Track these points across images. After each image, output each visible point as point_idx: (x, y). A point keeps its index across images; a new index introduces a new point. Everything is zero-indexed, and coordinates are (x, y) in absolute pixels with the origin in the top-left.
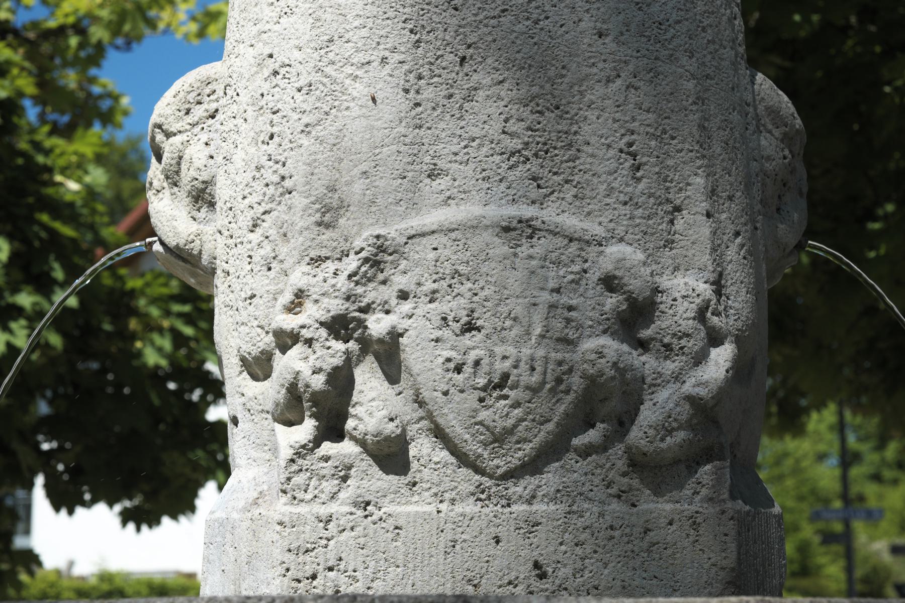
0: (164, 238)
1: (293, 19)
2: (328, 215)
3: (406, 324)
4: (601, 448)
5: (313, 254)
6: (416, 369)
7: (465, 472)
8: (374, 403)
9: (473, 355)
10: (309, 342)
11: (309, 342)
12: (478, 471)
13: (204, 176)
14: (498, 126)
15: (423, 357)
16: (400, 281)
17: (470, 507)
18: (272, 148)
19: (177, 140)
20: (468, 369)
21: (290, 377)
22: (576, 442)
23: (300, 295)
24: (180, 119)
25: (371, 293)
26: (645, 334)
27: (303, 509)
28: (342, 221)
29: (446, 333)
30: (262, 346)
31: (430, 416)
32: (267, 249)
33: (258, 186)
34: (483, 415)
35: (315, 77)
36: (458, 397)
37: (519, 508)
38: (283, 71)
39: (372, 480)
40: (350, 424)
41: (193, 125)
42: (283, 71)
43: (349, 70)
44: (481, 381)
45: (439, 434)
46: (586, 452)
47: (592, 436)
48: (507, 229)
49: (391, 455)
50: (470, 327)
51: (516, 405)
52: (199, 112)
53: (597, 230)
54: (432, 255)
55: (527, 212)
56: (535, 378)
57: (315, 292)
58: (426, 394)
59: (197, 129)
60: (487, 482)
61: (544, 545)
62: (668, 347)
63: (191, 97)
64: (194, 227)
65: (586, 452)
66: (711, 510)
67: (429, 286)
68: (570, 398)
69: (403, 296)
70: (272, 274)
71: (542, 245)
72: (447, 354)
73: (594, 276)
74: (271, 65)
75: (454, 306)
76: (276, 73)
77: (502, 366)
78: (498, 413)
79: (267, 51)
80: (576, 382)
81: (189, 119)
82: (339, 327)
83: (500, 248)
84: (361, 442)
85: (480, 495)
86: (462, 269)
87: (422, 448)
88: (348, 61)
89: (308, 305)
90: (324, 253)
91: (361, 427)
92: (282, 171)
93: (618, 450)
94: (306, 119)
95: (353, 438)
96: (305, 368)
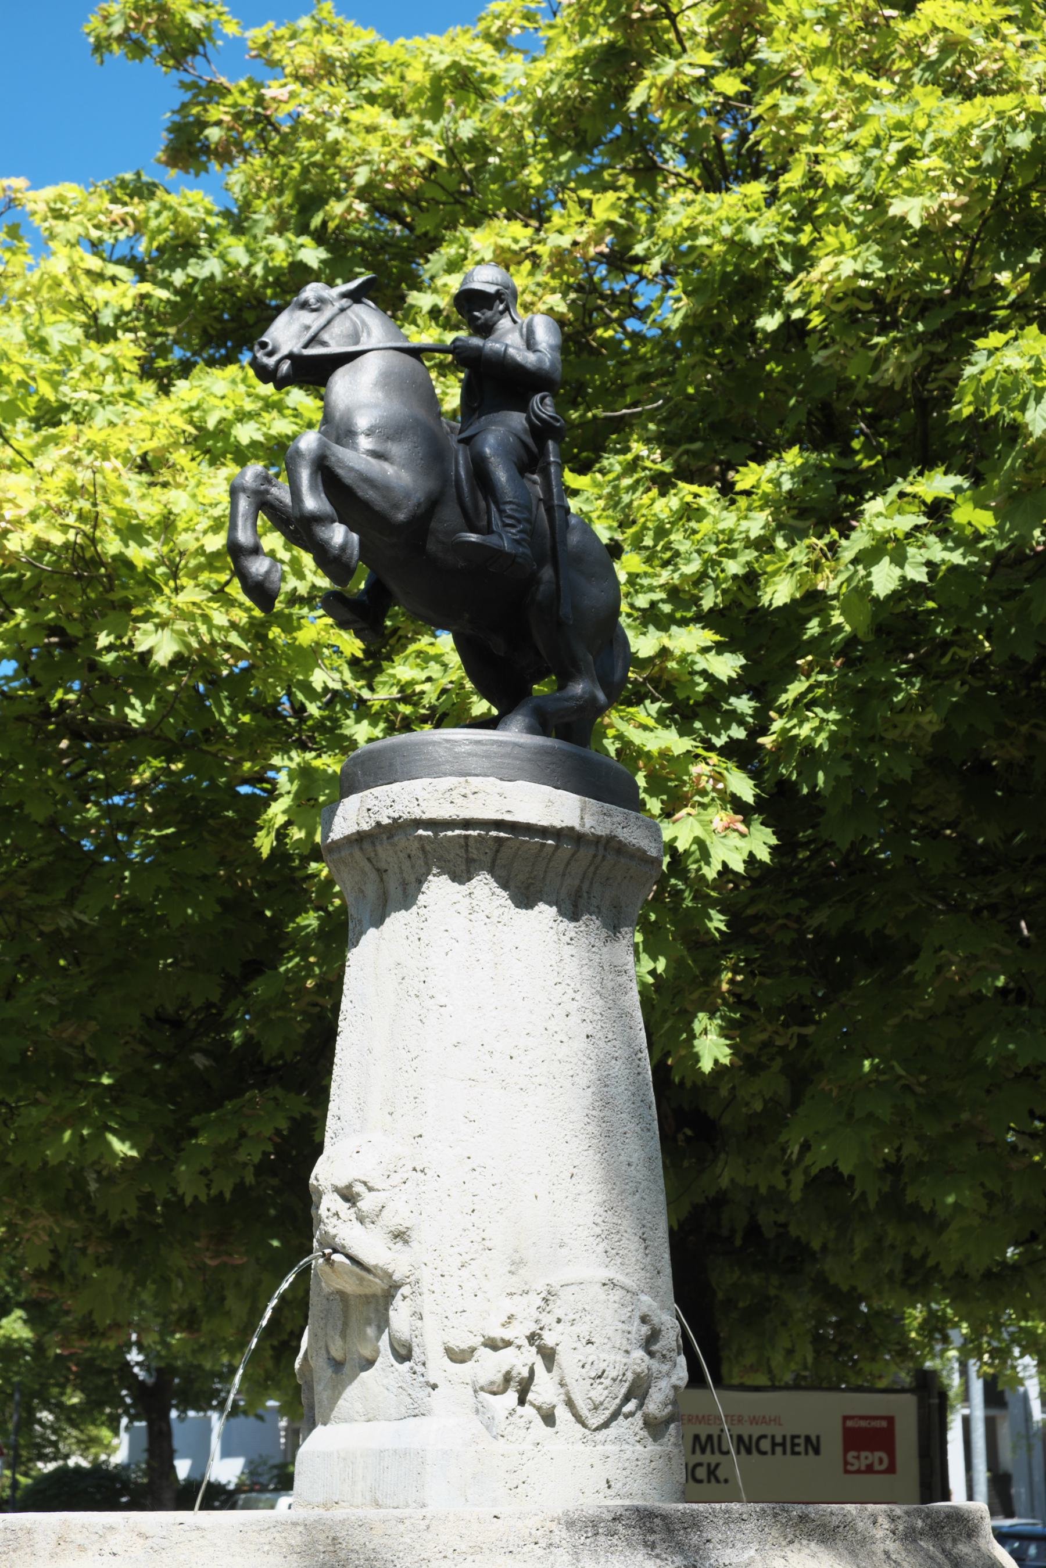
0: (354, 1251)
2: (516, 1265)
3: (561, 1338)
4: (631, 1414)
6: (564, 1365)
8: (544, 1390)
10: (519, 1347)
11: (519, 1347)
12: (584, 1425)
16: (559, 1313)
22: (626, 1409)
25: (547, 1319)
26: (654, 1348)
29: (578, 1345)
31: (567, 1394)
34: (593, 1394)
37: (600, 1447)
40: (530, 1396)
45: (570, 1403)
46: (631, 1414)
47: (631, 1406)
49: (549, 1419)
50: (589, 1342)
52: (396, 1179)
56: (614, 1374)
57: (520, 1316)
58: (568, 1380)
61: (611, 1470)
63: (391, 1167)
65: (627, 1416)
67: (571, 1317)
68: (627, 1385)
69: (559, 1321)
75: (583, 1329)
77: (603, 1366)
78: (599, 1393)
80: (630, 1376)
81: (390, 1181)
82: (532, 1338)
83: (601, 1293)
84: (539, 1409)
85: (584, 1441)
87: (562, 1413)
89: (515, 1322)
93: (639, 1414)
95: (532, 1404)
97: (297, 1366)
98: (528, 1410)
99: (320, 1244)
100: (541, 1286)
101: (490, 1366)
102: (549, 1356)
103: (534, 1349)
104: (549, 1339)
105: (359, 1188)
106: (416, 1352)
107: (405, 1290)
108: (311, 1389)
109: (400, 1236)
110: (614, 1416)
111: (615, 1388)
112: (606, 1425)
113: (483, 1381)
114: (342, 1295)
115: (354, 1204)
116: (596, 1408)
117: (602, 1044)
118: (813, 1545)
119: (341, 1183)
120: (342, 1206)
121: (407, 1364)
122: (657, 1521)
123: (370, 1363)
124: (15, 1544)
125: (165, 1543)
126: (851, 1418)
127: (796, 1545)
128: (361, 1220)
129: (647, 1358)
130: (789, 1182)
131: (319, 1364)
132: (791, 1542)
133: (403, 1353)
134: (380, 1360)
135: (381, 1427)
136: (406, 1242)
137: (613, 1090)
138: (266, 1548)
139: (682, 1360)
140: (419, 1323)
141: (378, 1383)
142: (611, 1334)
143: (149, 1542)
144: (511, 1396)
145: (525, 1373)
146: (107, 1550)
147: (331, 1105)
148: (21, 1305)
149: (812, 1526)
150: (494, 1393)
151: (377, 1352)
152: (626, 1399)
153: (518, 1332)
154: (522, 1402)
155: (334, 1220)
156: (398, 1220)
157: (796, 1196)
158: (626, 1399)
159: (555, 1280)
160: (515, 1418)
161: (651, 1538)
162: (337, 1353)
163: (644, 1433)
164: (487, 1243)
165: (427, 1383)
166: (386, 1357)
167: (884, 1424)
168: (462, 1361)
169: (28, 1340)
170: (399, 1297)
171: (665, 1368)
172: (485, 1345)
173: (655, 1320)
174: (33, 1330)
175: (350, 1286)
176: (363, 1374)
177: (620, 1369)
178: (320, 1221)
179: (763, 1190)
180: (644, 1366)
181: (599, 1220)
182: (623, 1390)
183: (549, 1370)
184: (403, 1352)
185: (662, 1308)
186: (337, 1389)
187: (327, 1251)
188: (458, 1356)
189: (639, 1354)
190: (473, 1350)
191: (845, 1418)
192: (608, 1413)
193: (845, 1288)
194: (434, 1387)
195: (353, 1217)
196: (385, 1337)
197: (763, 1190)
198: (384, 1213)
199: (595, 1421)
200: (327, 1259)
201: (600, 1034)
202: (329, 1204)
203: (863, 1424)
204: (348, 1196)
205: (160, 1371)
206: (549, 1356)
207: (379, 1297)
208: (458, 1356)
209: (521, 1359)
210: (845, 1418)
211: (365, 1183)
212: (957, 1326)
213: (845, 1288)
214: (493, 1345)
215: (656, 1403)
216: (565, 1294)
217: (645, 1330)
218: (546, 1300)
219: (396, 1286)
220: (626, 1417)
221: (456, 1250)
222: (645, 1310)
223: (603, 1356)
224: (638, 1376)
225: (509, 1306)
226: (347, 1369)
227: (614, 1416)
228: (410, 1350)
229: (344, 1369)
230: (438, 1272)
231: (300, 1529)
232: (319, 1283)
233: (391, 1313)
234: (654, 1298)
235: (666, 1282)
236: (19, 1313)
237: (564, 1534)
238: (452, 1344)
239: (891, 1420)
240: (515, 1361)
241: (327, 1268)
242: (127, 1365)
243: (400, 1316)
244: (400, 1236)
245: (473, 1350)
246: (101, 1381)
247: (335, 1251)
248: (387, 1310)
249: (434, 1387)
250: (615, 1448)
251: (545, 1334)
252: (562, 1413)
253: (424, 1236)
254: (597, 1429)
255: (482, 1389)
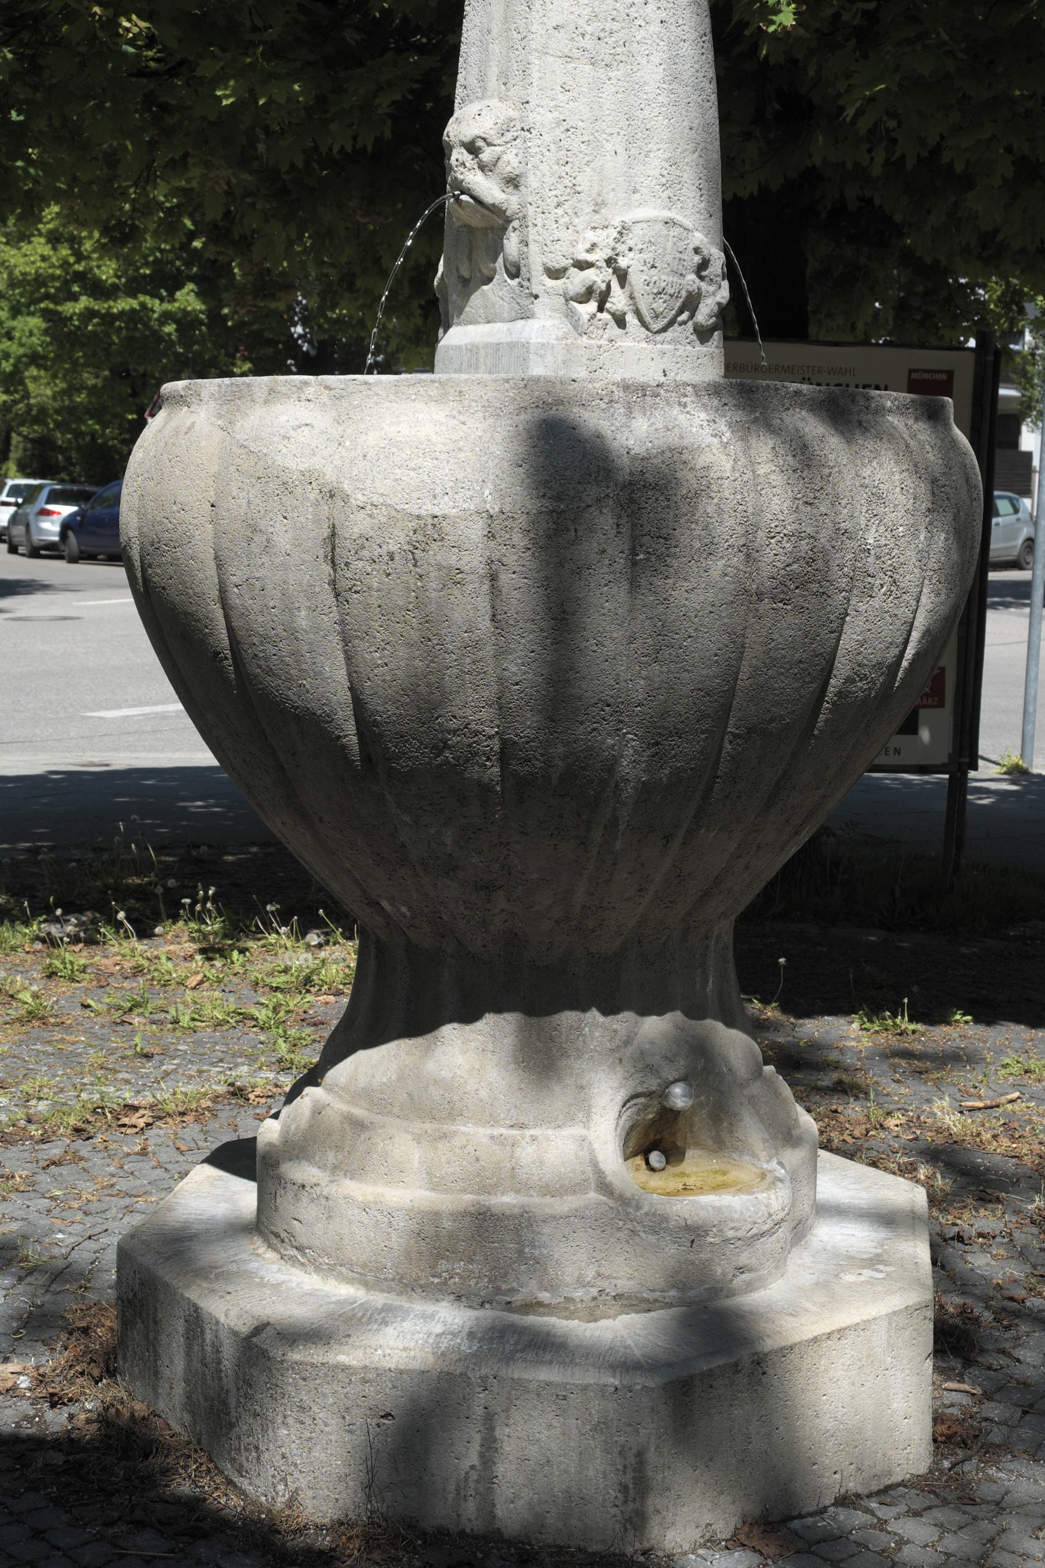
1: (577, 104)
3: (631, 262)
4: (685, 323)
5: (593, 225)
6: (634, 283)
7: (643, 329)
8: (618, 300)
9: (654, 279)
12: (648, 329)
13: (517, 172)
14: (659, 171)
15: (636, 279)
16: (630, 243)
17: (644, 345)
18: (567, 168)
19: (498, 149)
20: (651, 285)
21: (590, 283)
22: (680, 319)
23: (594, 246)
24: (499, 138)
25: (621, 248)
26: (704, 273)
27: (592, 342)
28: (603, 211)
29: (645, 268)
30: (563, 265)
31: (635, 304)
32: (566, 219)
33: (561, 187)
34: (654, 306)
35: (592, 138)
36: (646, 296)
37: (659, 346)
38: (572, 130)
39: (614, 330)
40: (608, 305)
41: (507, 143)
42: (572, 130)
43: (604, 136)
44: (655, 291)
45: (638, 313)
46: (685, 323)
47: (684, 316)
48: (666, 223)
49: (620, 321)
50: (653, 266)
51: (665, 302)
52: (509, 136)
53: (690, 226)
54: (641, 232)
55: (673, 214)
56: (672, 291)
59: (509, 145)
60: (650, 334)
62: (711, 280)
63: (504, 127)
64: (504, 196)
66: (717, 351)
67: (640, 246)
68: (681, 300)
69: (630, 249)
70: (570, 231)
71: (677, 231)
72: (645, 277)
73: (691, 246)
74: (565, 125)
75: (648, 256)
76: (568, 130)
77: (663, 284)
78: (659, 305)
79: (562, 118)
80: (684, 294)
81: (504, 139)
82: (610, 262)
84: (613, 315)
86: (652, 240)
87: (631, 319)
88: (604, 131)
89: (597, 250)
90: (596, 225)
91: (614, 308)
92: (574, 181)
93: (690, 323)
94: (587, 158)
95: (609, 312)
96: (599, 280)
97: (435, 283)
98: (605, 316)
99: (451, 187)
100: (617, 221)
101: (577, 280)
102: (622, 276)
103: (610, 270)
104: (623, 262)
105: (480, 143)
106: (523, 270)
107: (516, 224)
108: (446, 301)
109: (513, 182)
110: (671, 323)
111: (672, 302)
112: (664, 329)
113: (571, 293)
114: (470, 229)
115: (477, 156)
116: (657, 317)
117: (673, 28)
118: (803, 412)
119: (467, 140)
120: (467, 157)
121: (517, 280)
122: (689, 388)
123: (489, 280)
124: (238, 395)
125: (344, 393)
126: (916, 371)
127: (791, 411)
128: (482, 167)
129: (697, 280)
130: (872, 159)
131: (452, 281)
132: (788, 409)
133: (514, 271)
134: (497, 277)
135: (499, 326)
136: (516, 187)
137: (680, 67)
138: (413, 397)
139: (725, 284)
140: (525, 249)
141: (496, 292)
142: (670, 261)
143: (333, 392)
144: (592, 306)
145: (603, 286)
146: (303, 397)
147: (459, 77)
148: (192, 279)
149: (804, 399)
150: (581, 303)
151: (495, 271)
152: (681, 312)
153: (598, 256)
154: (601, 309)
155: (461, 169)
156: (509, 169)
157: (877, 171)
158: (681, 312)
159: (629, 217)
160: (595, 321)
161: (684, 400)
162: (466, 274)
163: (694, 337)
164: (578, 188)
165: (531, 294)
166: (501, 275)
167: (944, 377)
168: (557, 278)
169: (201, 312)
170: (510, 228)
171: (712, 289)
172: (574, 266)
173: (705, 252)
174: (204, 303)
175: (476, 222)
176: (485, 287)
177: (677, 288)
178: (451, 168)
179: (849, 166)
180: (695, 286)
181: (665, 173)
182: (678, 304)
183: (622, 286)
184: (513, 270)
185: (712, 243)
186: (467, 296)
187: (457, 193)
188: (555, 274)
189: (692, 277)
190: (565, 270)
191: (911, 371)
192: (666, 320)
193: (928, 260)
194: (536, 297)
195: (476, 166)
196: (500, 260)
197: (849, 166)
198: (500, 163)
199: (656, 326)
200: (457, 198)
201: (672, 20)
202: (458, 155)
203: (926, 376)
204: (472, 148)
205: (321, 343)
206: (622, 276)
207: (495, 223)
208: (555, 274)
209: (599, 277)
210: (911, 371)
211: (484, 139)
212: (1033, 299)
213: (928, 260)
214: (582, 265)
215: (705, 313)
216: (637, 230)
217: (697, 259)
218: (620, 233)
219: (508, 221)
220: (680, 325)
221: (554, 193)
222: (697, 243)
223: (663, 277)
224: (690, 294)
225: (591, 236)
226: (472, 285)
227: (671, 323)
228: (518, 269)
229: (468, 285)
230: (539, 210)
231: (437, 385)
232: (451, 219)
233: (505, 241)
234: (706, 236)
235: (716, 223)
236: (191, 286)
237: (621, 394)
238: (550, 264)
239: (950, 374)
240: (596, 278)
241: (457, 207)
242: (291, 340)
243: (511, 244)
244: (513, 182)
245: (565, 270)
246: (270, 351)
247: (463, 193)
248: (502, 239)
249: (536, 297)
250: (671, 347)
251: (620, 259)
252: (631, 319)
253: (532, 181)
254: (659, 332)
255: (572, 299)
